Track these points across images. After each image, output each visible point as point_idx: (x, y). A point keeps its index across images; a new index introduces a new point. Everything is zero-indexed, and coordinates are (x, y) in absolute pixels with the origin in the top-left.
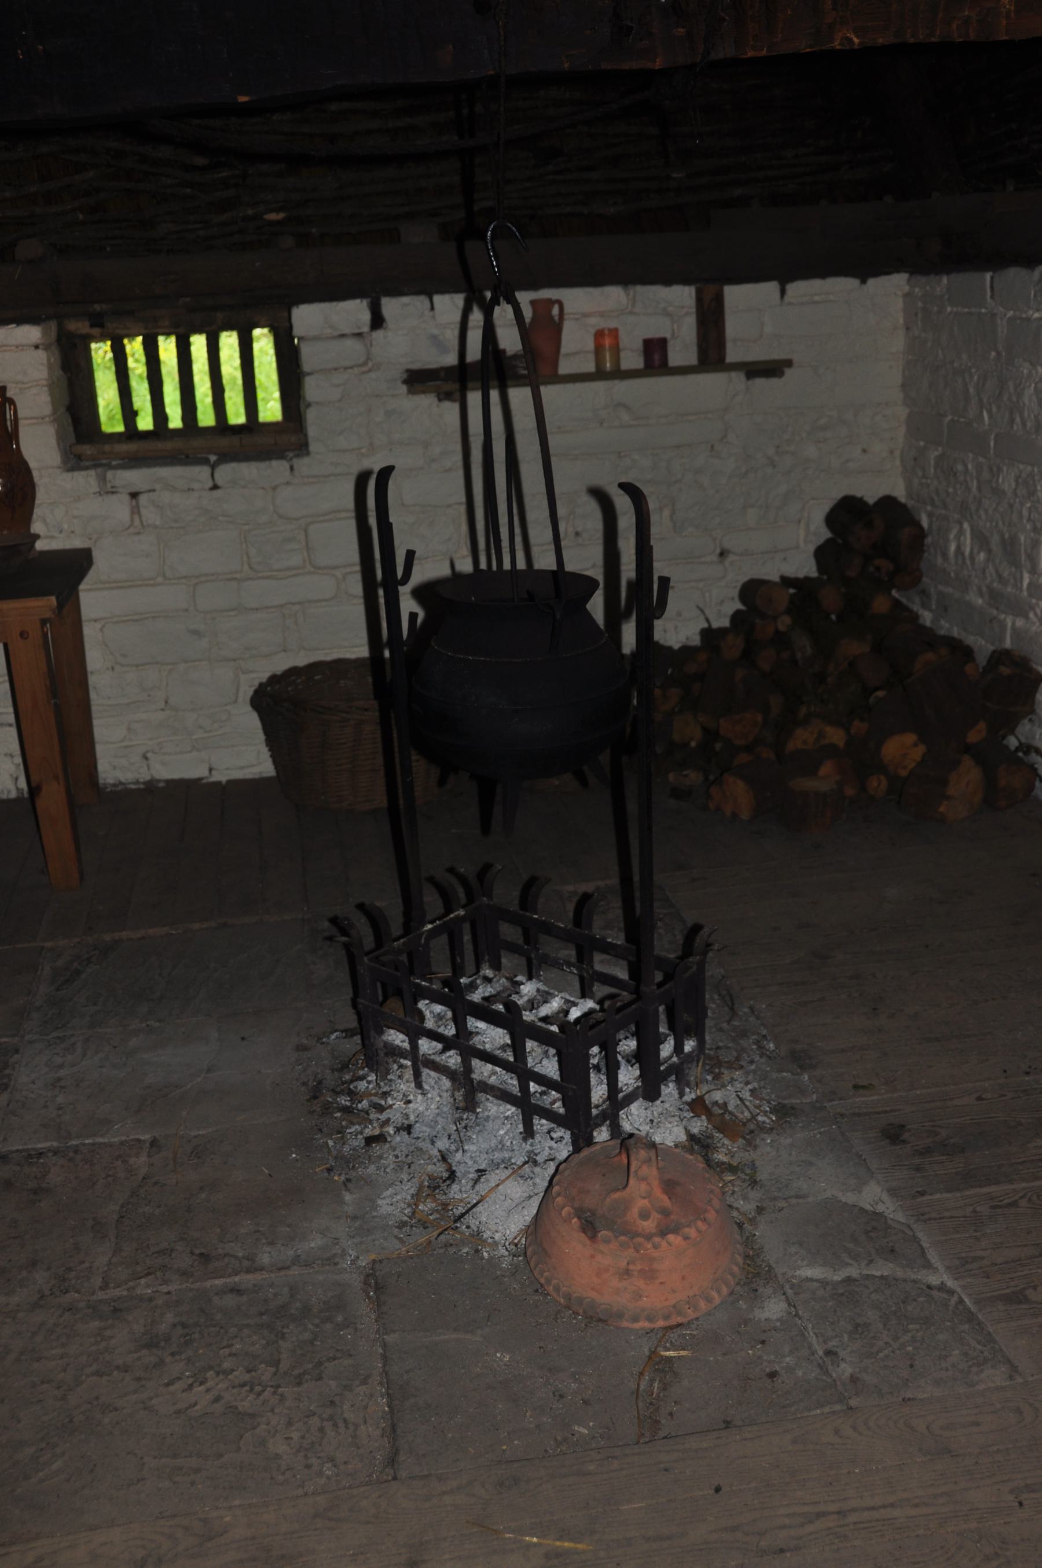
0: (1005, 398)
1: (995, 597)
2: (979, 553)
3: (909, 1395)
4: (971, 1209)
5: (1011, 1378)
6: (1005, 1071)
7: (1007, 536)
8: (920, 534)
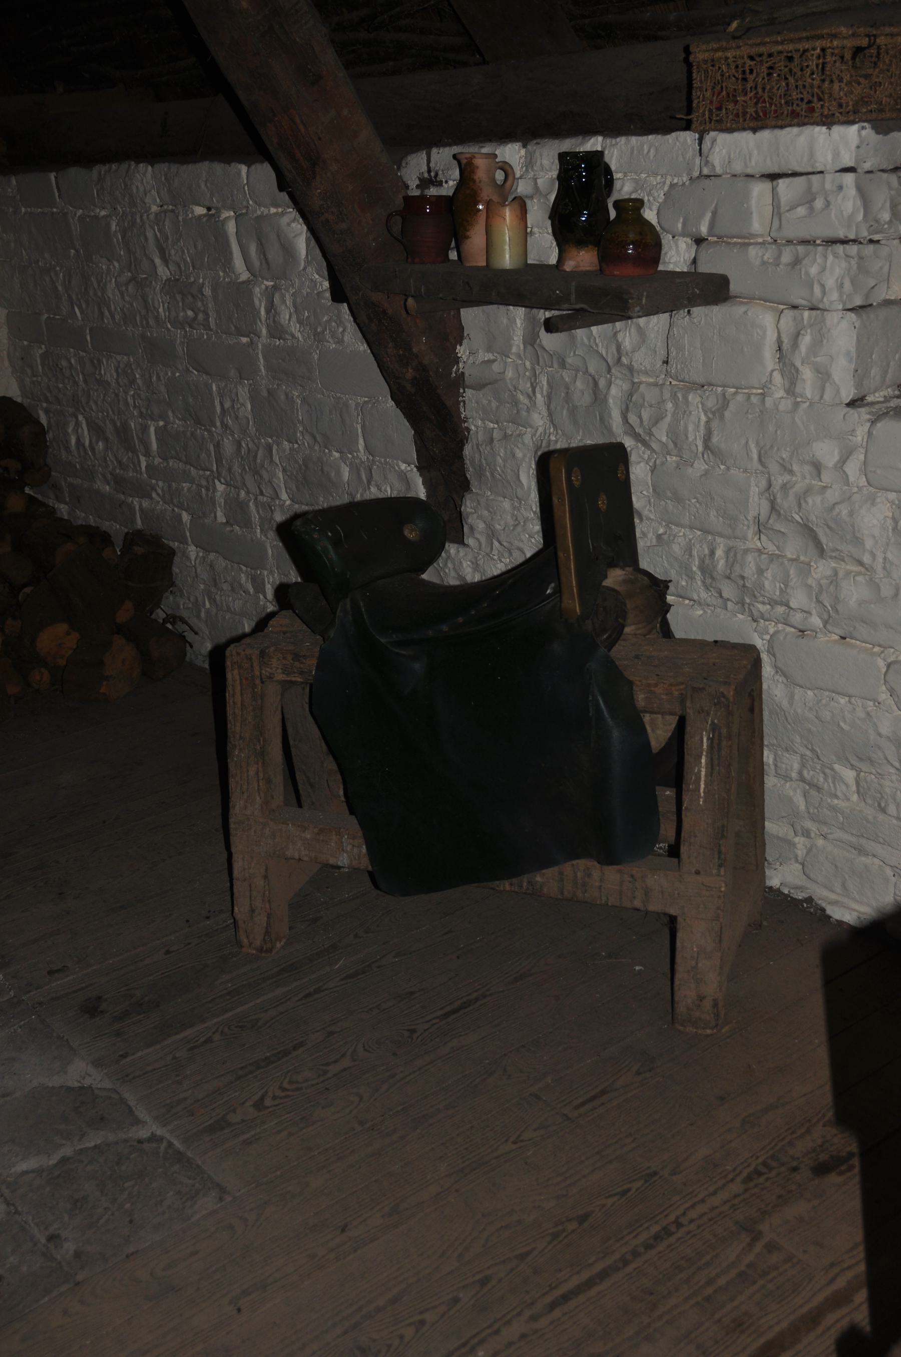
0: (91, 293)
1: (119, 482)
2: (97, 443)
3: (132, 1249)
4: (171, 1056)
5: (221, 1199)
6: (188, 921)
7: (118, 424)
8: (40, 432)
